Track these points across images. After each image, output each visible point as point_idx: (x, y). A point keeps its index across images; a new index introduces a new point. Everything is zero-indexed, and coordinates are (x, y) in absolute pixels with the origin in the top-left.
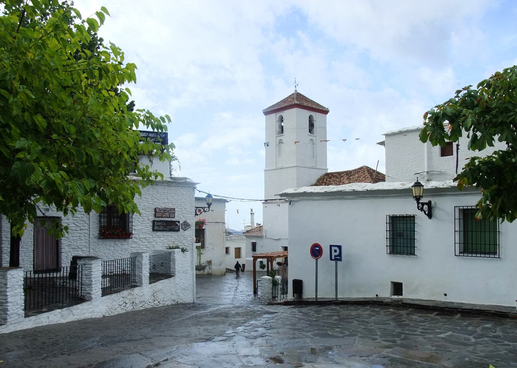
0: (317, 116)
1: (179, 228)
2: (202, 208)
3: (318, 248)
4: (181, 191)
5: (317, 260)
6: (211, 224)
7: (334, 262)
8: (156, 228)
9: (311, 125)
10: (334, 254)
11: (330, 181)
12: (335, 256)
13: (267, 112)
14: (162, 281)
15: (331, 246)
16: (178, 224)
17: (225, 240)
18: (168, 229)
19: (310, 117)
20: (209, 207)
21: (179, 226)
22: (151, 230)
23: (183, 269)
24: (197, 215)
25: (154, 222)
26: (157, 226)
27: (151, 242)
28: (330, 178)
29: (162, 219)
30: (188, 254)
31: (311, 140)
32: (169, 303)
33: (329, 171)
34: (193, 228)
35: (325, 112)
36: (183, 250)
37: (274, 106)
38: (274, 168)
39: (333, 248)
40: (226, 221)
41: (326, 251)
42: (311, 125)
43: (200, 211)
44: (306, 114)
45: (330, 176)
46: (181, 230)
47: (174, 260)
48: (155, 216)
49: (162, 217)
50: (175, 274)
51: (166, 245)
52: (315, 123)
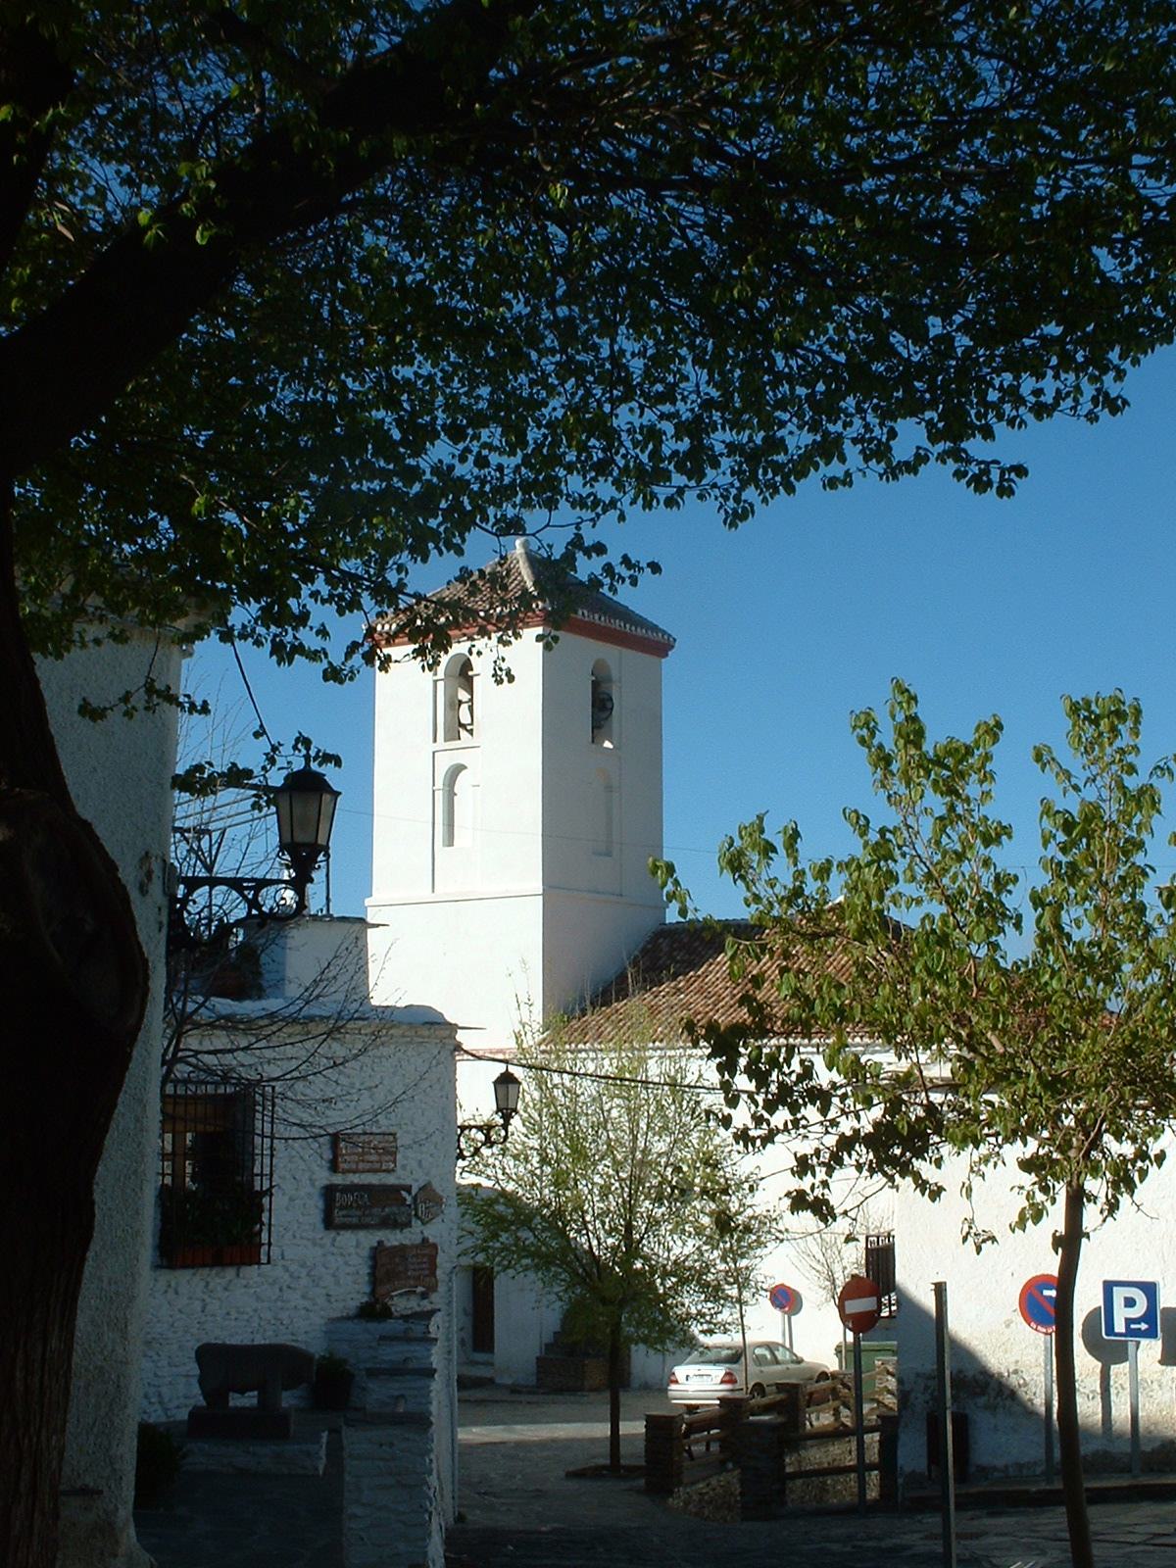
8: (338, 1216)
9: (602, 705)
22: (320, 1226)
25: (329, 1192)
26: (342, 1208)
35: (659, 645)
39: (1119, 1295)
48: (334, 1167)
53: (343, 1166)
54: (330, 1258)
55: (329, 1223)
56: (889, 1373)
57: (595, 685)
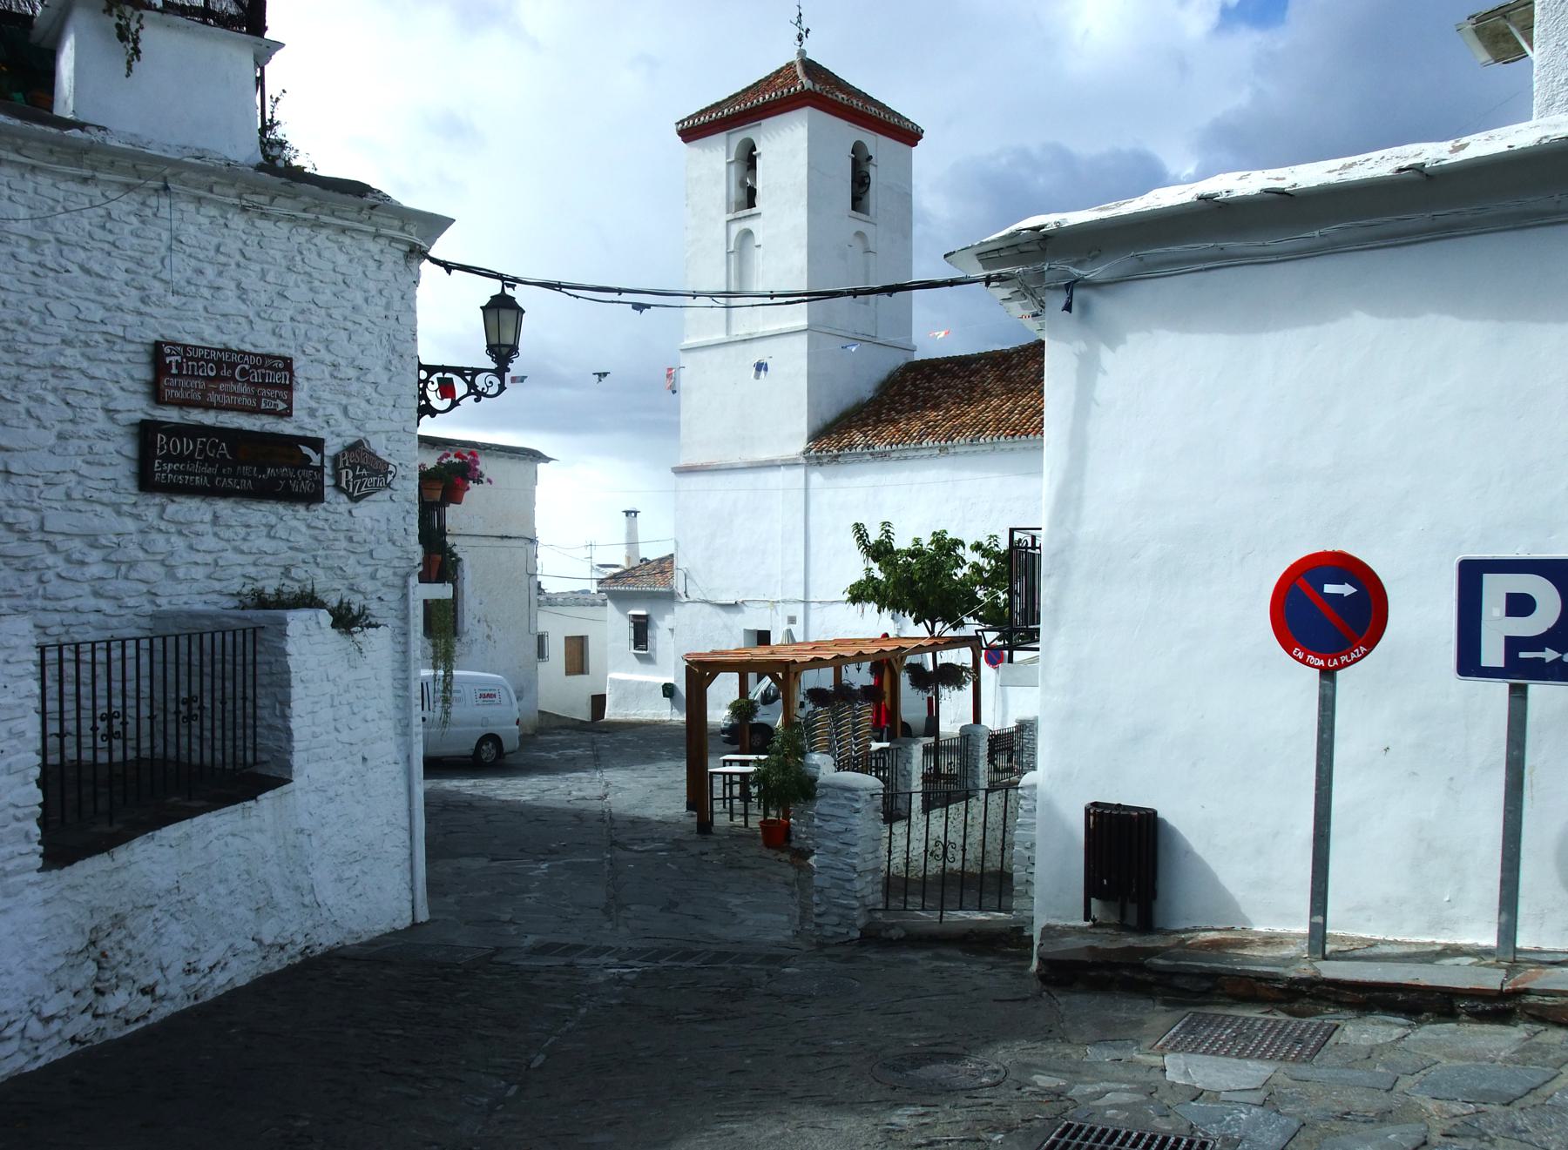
0: (877, 144)
1: (321, 483)
2: (459, 371)
3: (1347, 590)
4: (334, 253)
5: (1328, 674)
6: (484, 542)
7: (1499, 690)
8: (163, 471)
9: (860, 183)
10: (1496, 628)
11: (930, 389)
12: (1513, 645)
13: (692, 132)
14: (172, 832)
15: (1471, 574)
16: (316, 460)
17: (534, 603)
18: (246, 484)
19: (858, 148)
20: (500, 372)
21: (320, 469)
22: (129, 484)
23: (345, 736)
24: (434, 413)
25: (146, 432)
26: (168, 458)
27: (132, 565)
28: (929, 378)
29: (209, 418)
30: (378, 643)
31: (859, 234)
32: (241, 973)
33: (918, 357)
34: (408, 488)
35: (909, 135)
36: (346, 620)
37: (717, 106)
38: (721, 336)
39: (1495, 589)
40: (540, 535)
41: (1421, 614)
42: (860, 183)
43: (446, 389)
44: (849, 133)
45: (927, 370)
46: (329, 493)
47: (282, 681)
48: (157, 396)
49: (207, 407)
50: (288, 766)
51: (235, 586)
52: (872, 171)
53: (168, 393)
54: (154, 535)
55: (147, 482)
56: (511, 922)
57: (856, 164)
